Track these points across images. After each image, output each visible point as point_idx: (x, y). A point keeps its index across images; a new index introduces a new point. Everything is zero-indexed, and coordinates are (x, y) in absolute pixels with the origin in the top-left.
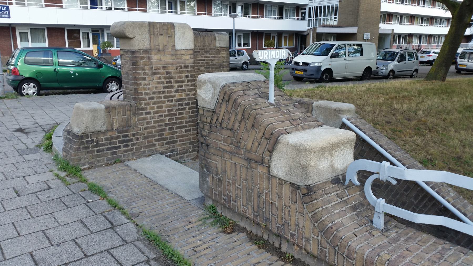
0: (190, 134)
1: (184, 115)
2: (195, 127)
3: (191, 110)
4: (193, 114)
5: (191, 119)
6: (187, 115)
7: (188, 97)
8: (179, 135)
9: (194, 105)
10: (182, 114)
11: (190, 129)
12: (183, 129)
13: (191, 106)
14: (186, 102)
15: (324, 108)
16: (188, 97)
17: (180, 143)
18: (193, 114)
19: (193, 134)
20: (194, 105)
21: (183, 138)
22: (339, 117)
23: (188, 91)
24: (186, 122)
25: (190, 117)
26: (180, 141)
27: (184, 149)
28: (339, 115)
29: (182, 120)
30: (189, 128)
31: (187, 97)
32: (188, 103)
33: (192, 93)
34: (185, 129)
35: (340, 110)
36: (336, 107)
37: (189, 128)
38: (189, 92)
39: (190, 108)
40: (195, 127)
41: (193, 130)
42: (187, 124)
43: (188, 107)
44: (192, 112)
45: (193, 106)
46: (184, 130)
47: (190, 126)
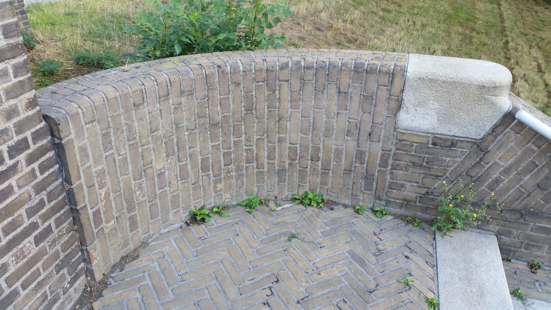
0: (54, 241)
1: (17, 192)
2: (62, 212)
3: (35, 165)
4: (47, 174)
5: (44, 195)
6: (29, 188)
7: (15, 120)
8: (18, 270)
9: (45, 142)
10: (37, 274)
11: (50, 225)
12: (27, 240)
13: (33, 147)
14: (11, 143)
15: (444, 82)
16: (15, 120)
17: (26, 291)
18: (47, 174)
19: (60, 237)
20: (45, 142)
21: (35, 268)
22: (493, 104)
23: (8, 99)
24: (31, 212)
25: (39, 189)
26: (24, 287)
27: (46, 297)
28: (493, 98)
29: (11, 214)
30: (46, 224)
31: (10, 125)
32: (18, 143)
33: (25, 102)
34: (31, 238)
35: (495, 88)
36: (484, 80)
37: (46, 224)
38: (13, 102)
39: (30, 160)
40: (62, 212)
41: (59, 222)
42: (34, 219)
43: (22, 157)
44: (43, 168)
45: (39, 144)
46: (28, 242)
47: (45, 217)
